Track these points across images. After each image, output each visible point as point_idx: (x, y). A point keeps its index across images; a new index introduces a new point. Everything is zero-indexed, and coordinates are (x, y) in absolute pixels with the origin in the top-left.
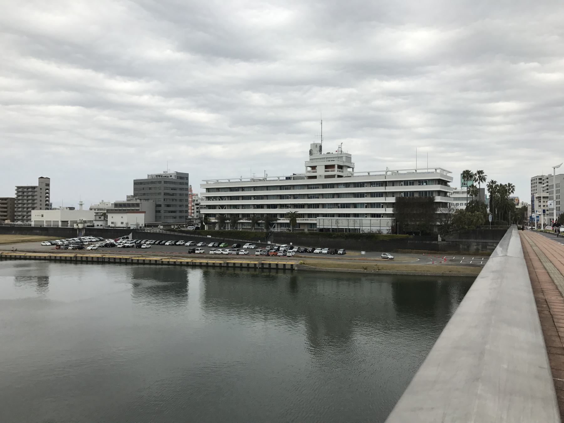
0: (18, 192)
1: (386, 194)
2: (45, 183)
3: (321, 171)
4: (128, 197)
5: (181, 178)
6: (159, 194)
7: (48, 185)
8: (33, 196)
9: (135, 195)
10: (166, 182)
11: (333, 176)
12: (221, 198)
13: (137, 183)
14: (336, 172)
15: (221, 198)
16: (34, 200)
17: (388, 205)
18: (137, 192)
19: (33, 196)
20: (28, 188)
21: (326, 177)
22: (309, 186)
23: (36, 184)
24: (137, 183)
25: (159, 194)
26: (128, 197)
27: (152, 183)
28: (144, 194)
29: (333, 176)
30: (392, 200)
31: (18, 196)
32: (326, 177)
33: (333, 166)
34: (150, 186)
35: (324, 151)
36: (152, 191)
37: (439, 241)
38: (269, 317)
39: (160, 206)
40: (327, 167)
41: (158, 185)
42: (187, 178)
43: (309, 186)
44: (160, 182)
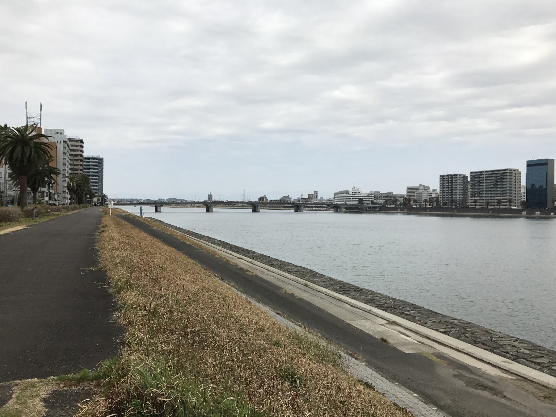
7: (317, 194)
17: (357, 201)
20: (311, 195)
23: (313, 193)
30: (358, 200)
42: (349, 192)
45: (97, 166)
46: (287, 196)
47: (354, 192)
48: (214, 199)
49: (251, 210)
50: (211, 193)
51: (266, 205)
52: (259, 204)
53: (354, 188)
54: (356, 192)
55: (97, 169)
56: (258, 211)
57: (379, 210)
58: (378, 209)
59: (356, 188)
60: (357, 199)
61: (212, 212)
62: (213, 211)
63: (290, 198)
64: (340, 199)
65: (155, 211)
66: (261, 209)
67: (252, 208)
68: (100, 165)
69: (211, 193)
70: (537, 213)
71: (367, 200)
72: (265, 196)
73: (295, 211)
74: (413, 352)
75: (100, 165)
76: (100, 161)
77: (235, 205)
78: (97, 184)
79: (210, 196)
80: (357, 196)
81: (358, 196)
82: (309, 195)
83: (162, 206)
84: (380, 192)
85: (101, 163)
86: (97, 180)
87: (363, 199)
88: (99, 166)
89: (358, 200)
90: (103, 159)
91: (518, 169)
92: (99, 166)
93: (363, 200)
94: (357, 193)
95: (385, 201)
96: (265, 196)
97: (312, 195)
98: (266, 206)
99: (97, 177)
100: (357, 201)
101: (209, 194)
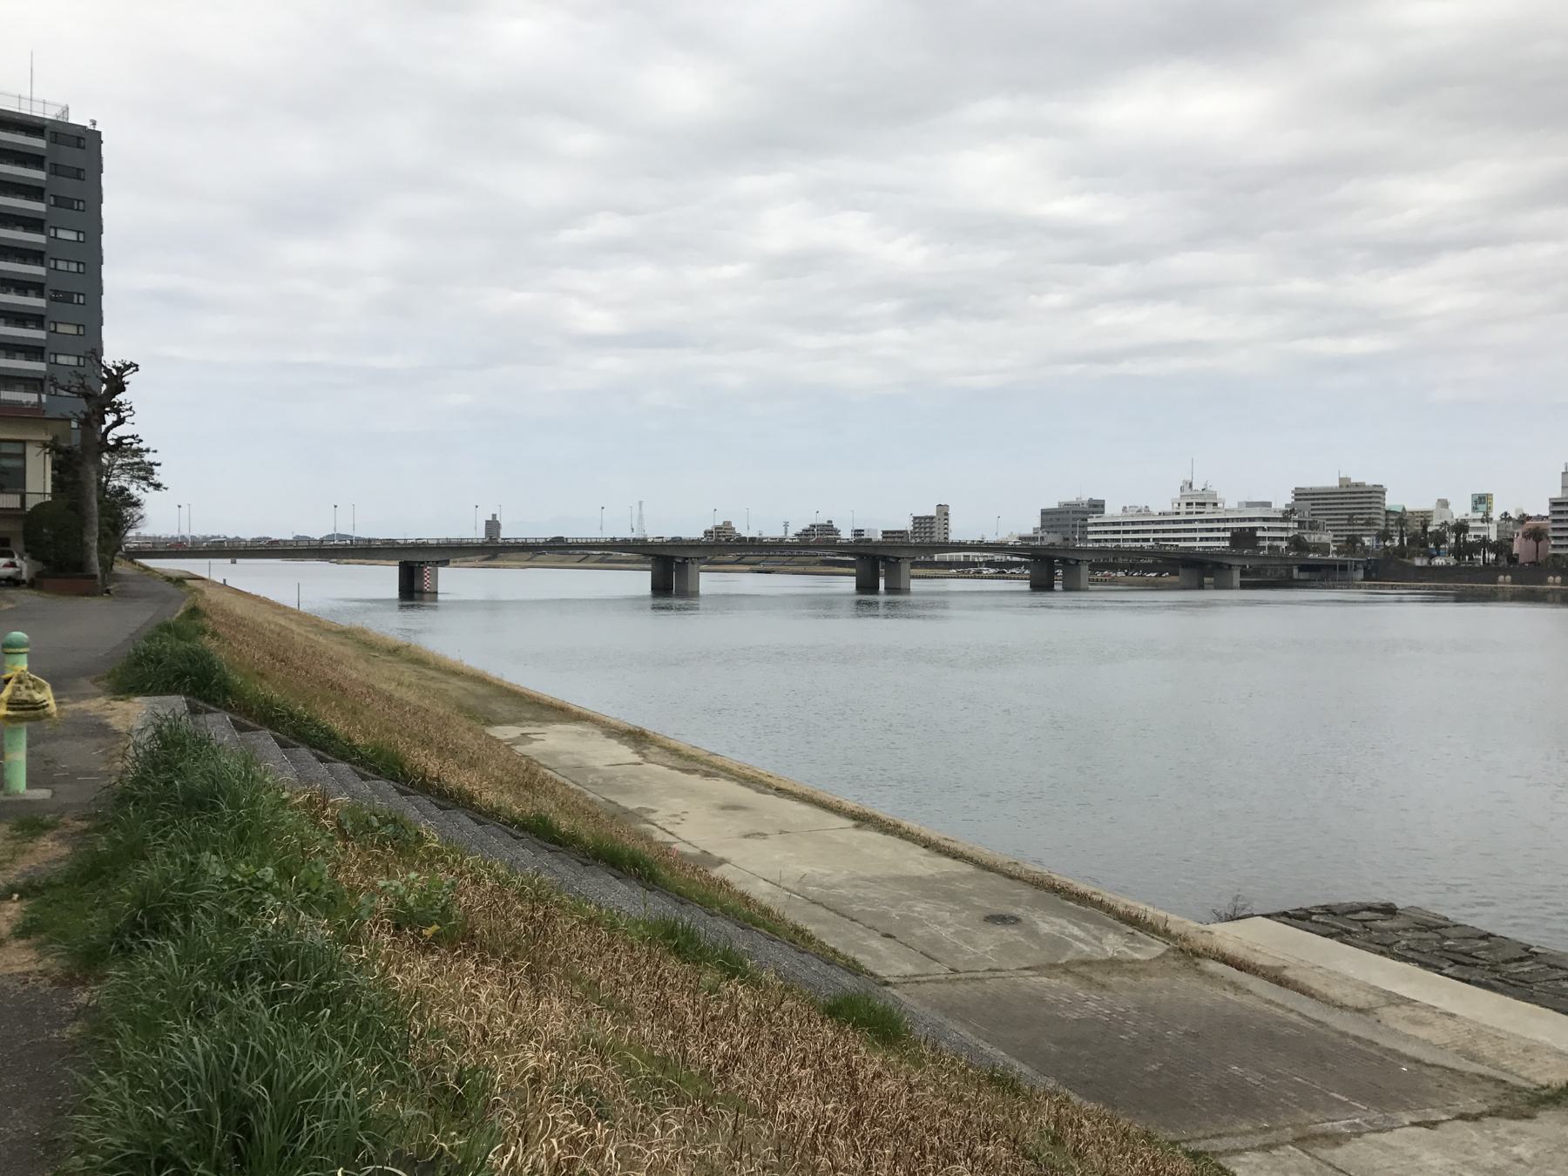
0: (915, 523)
1: (1342, 536)
2: (943, 510)
3: (1183, 508)
4: (1034, 529)
5: (1095, 506)
6: (1067, 526)
7: (946, 514)
8: (931, 528)
9: (1042, 527)
10: (1074, 512)
11: (1192, 513)
12: (1106, 532)
13: (1044, 513)
14: (1194, 508)
15: (1106, 532)
16: (932, 533)
17: (1224, 539)
18: (1045, 523)
19: (931, 528)
20: (926, 518)
21: (1187, 513)
22: (1174, 522)
23: (933, 513)
24: (1044, 513)
25: (1067, 526)
26: (1034, 529)
27: (1062, 512)
28: (1052, 526)
29: (1192, 513)
30: (1228, 534)
31: (915, 528)
32: (1187, 513)
33: (1191, 504)
34: (1058, 516)
35: (1194, 488)
36: (1060, 523)
37: (28, 490)
38: (151, 545)
39: (1068, 539)
40: (1188, 504)
41: (1065, 516)
42: (1103, 506)
43: (1174, 522)
44: (1068, 512)
45: (34, 192)
46: (825, 523)
47: (1197, 504)
48: (507, 533)
49: (1025, 586)
50: (494, 516)
51: (743, 557)
52: (905, 554)
53: (1191, 485)
54: (1204, 504)
55: (37, 319)
56: (903, 586)
57: (1363, 580)
58: (1362, 572)
59: (1197, 486)
60: (1224, 530)
61: (696, 594)
62: (701, 592)
63: (837, 532)
64: (1175, 531)
65: (394, 592)
66: (914, 577)
67: (650, 566)
68: (67, 187)
69: (494, 516)
70: (1501, 578)
71: (1274, 537)
72: (729, 523)
73: (1033, 586)
74: (720, 868)
75: (67, 187)
76: (69, 157)
77: (610, 558)
78: (40, 334)
79: (493, 526)
80: (1219, 520)
81: (1227, 520)
82: (915, 518)
83: (445, 563)
84: (1378, 492)
85: (77, 174)
86: (40, 295)
87: (1255, 529)
88: (61, 202)
89: (1228, 534)
90: (96, 137)
91: (487, 521)
92: (61, 202)
93: (1259, 534)
94: (1209, 508)
95: (1348, 541)
96: (729, 523)
97: (932, 518)
98: (743, 560)
99: (40, 303)
100: (1224, 539)
101: (490, 519)
